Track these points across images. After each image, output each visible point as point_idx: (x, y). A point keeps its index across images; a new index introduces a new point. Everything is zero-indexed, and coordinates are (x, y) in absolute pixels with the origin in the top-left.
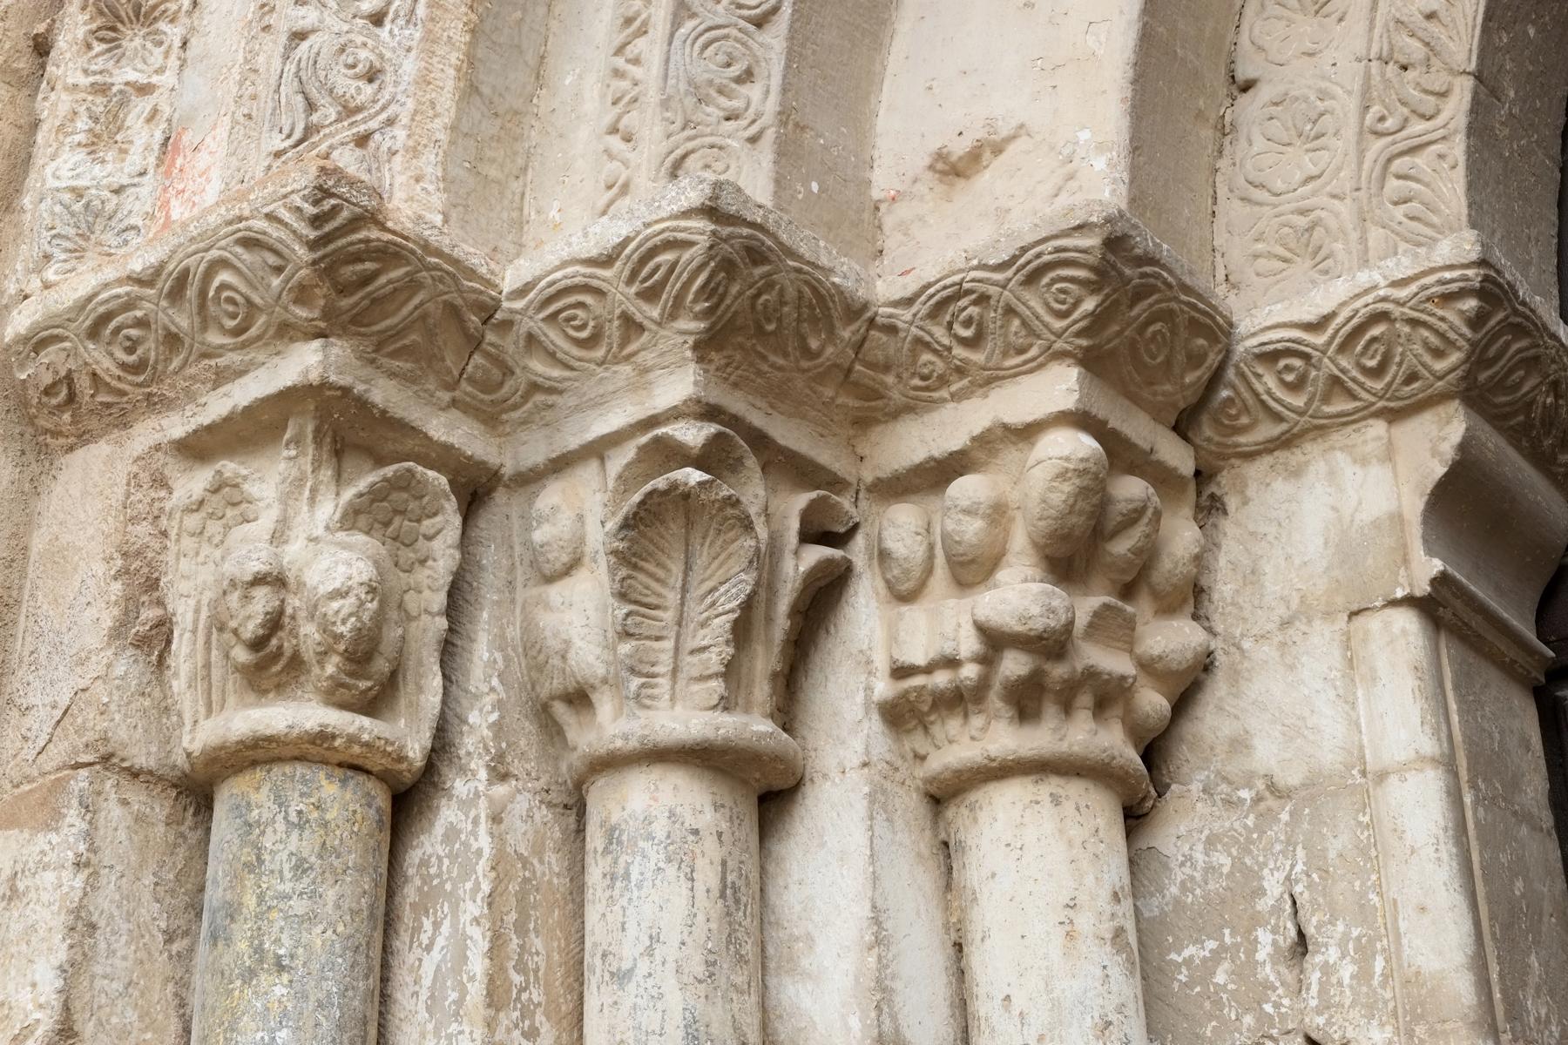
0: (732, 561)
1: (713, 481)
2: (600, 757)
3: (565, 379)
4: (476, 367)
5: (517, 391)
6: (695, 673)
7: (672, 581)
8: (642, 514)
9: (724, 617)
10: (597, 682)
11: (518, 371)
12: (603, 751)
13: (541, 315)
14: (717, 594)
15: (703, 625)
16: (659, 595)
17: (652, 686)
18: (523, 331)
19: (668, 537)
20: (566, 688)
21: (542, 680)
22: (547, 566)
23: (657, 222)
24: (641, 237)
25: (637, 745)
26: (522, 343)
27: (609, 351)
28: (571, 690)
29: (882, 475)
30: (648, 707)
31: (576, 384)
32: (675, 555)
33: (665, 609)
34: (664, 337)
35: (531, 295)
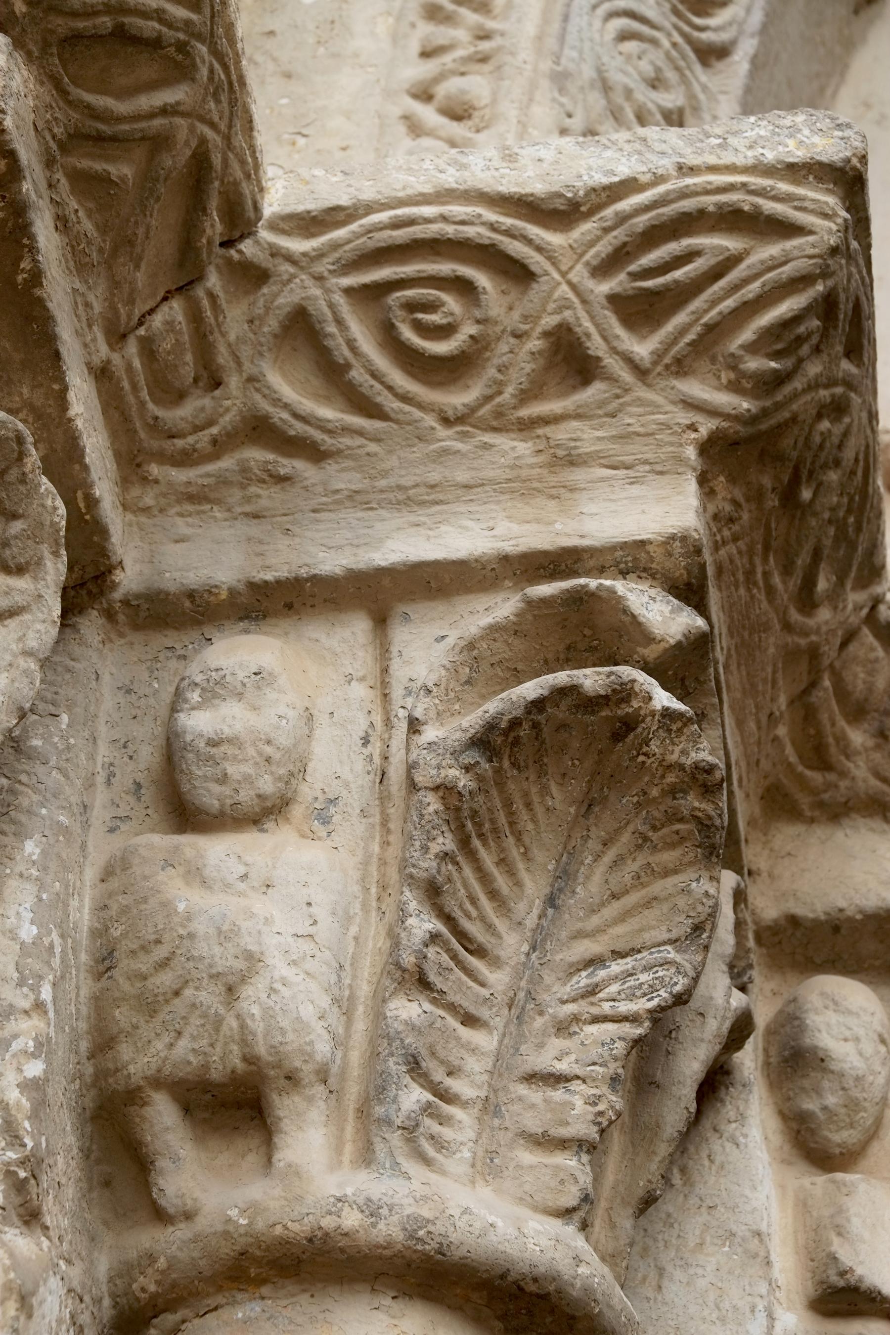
0: (650, 915)
1: (690, 719)
2: (284, 1242)
3: (347, 430)
4: (170, 324)
5: (210, 423)
6: (533, 1124)
7: (520, 908)
8: (524, 731)
9: (610, 1027)
10: (307, 1071)
11: (234, 382)
12: (299, 1229)
13: (347, 281)
14: (602, 974)
15: (563, 1028)
16: (490, 927)
17: (443, 1120)
18: (287, 299)
19: (539, 810)
20: (206, 1067)
21: (146, 1031)
22: (216, 788)
23: (713, 169)
24: (661, 189)
25: (398, 1235)
26: (272, 324)
27: (488, 399)
28: (216, 1075)
29: (800, 911)
30: (427, 1161)
31: (373, 447)
32: (539, 855)
33: (496, 963)
34: (641, 402)
35: (340, 233)
